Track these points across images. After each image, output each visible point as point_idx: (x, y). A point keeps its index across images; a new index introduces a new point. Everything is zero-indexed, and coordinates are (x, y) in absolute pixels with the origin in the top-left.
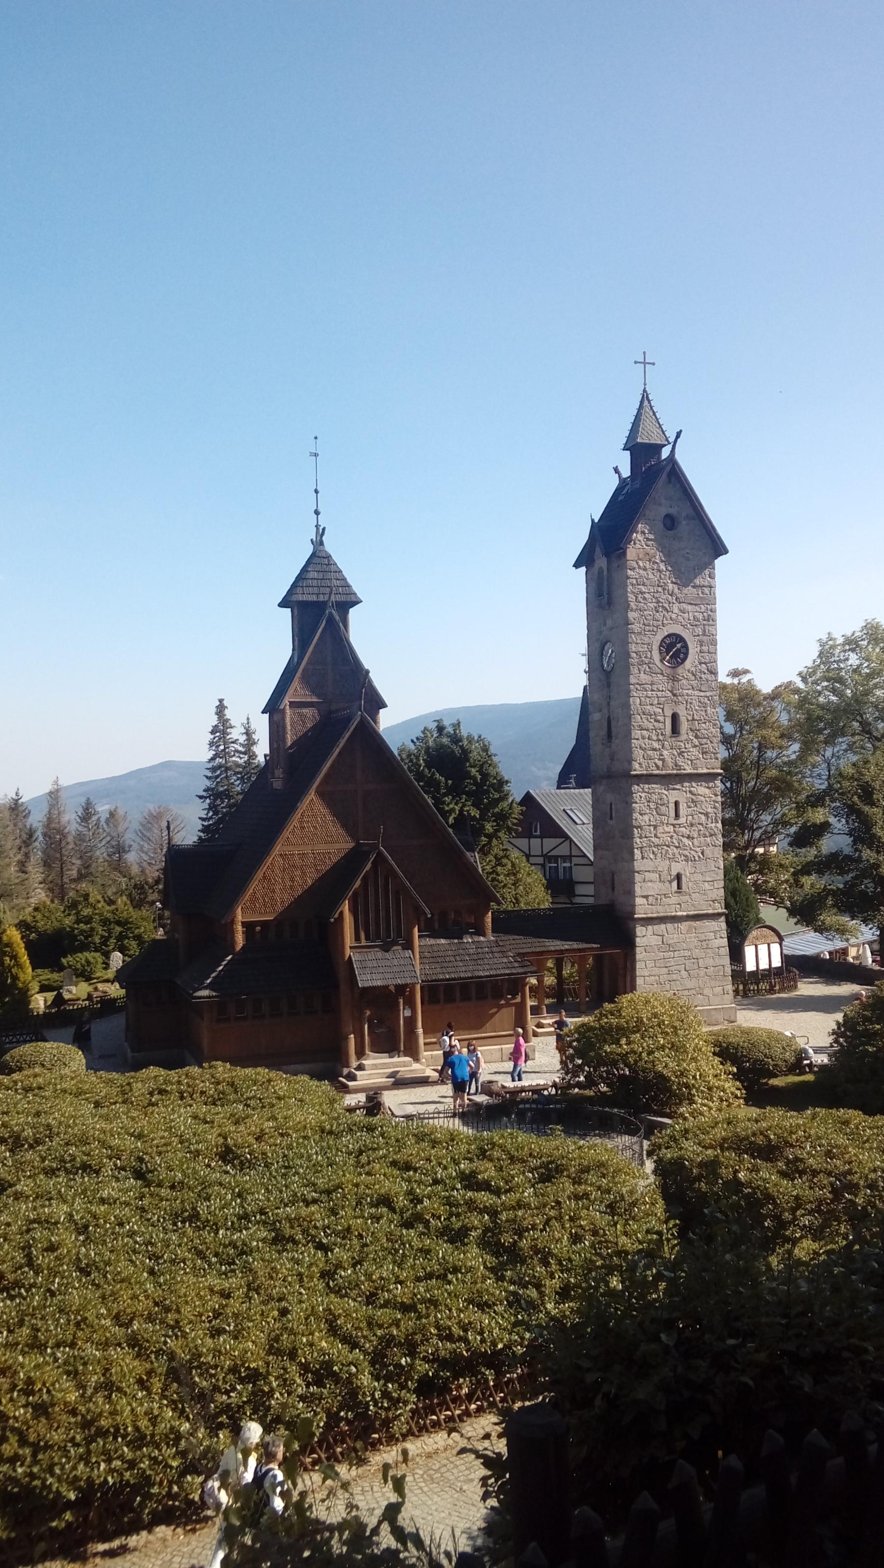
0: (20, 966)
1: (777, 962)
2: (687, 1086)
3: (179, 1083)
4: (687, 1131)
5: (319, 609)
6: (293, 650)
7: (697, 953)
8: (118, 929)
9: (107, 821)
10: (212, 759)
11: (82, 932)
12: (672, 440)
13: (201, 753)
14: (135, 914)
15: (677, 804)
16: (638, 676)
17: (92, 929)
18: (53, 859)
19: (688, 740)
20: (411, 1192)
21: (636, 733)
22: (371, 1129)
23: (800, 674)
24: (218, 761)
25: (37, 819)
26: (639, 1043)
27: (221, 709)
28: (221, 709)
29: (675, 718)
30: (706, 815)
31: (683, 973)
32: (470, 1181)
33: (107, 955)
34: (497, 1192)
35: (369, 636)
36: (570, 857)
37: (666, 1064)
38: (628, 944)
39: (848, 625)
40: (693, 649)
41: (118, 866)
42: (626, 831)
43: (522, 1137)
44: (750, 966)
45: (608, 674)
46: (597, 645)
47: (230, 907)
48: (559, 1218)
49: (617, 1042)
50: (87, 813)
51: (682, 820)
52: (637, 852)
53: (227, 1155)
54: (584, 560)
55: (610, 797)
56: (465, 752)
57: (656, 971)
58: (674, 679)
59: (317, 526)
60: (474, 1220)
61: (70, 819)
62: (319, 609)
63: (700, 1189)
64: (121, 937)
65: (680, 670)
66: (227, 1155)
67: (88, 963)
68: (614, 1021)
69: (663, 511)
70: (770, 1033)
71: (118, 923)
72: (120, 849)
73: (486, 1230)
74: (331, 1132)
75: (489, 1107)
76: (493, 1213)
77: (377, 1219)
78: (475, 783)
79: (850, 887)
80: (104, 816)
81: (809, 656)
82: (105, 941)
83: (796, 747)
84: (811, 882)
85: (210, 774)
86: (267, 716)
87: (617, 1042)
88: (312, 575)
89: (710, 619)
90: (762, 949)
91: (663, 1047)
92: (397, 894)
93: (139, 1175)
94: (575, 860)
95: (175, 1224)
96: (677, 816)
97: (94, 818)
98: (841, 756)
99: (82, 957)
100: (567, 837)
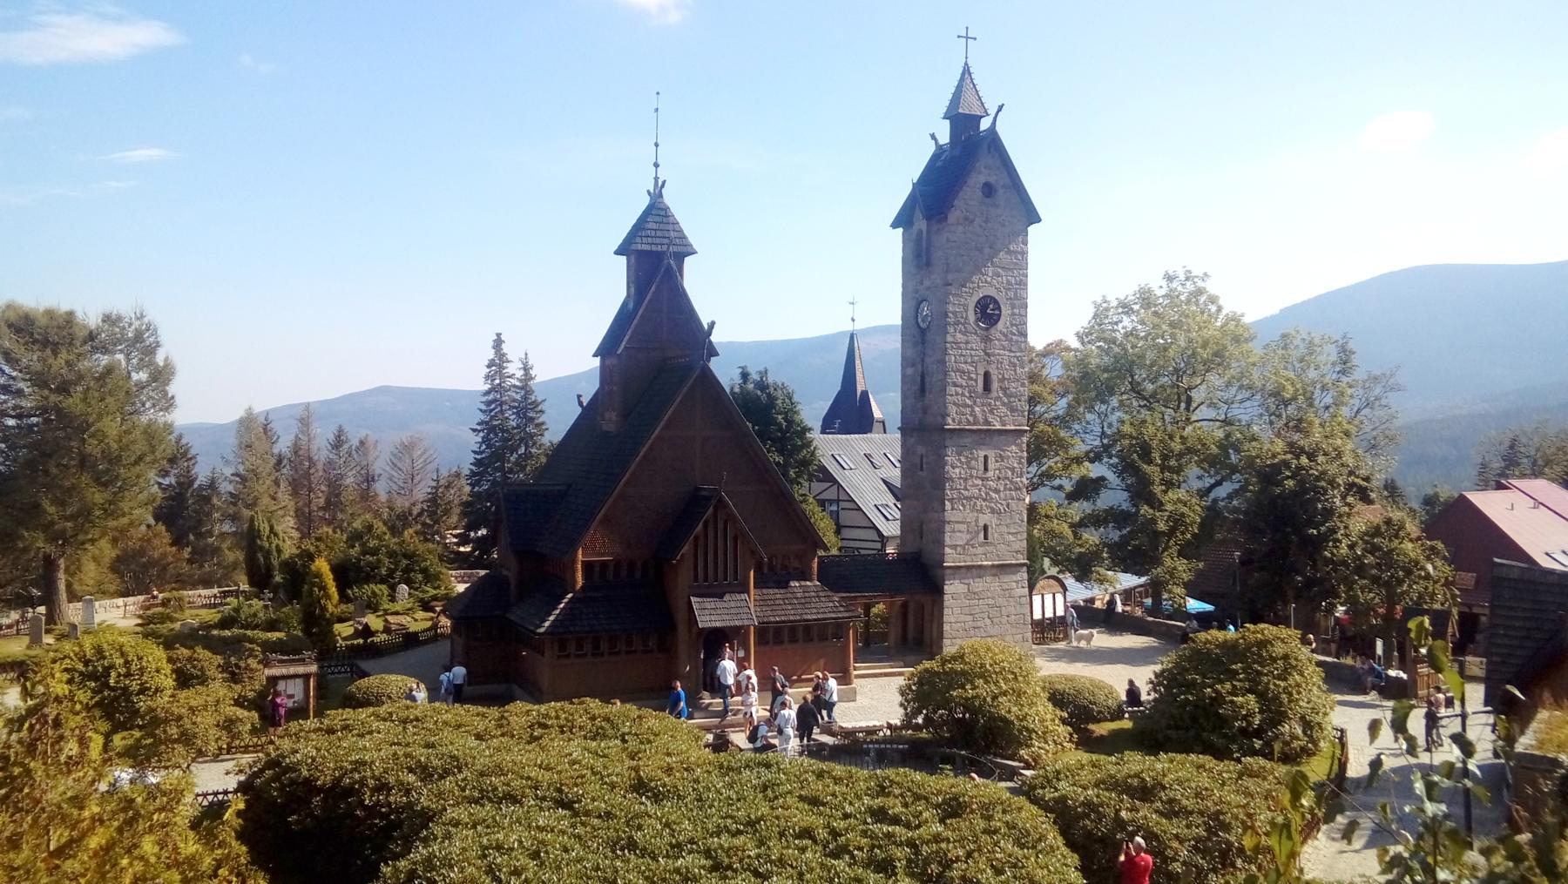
0: (328, 597)
1: (1060, 612)
2: (1027, 729)
3: (557, 717)
4: (1058, 772)
5: (655, 255)
6: (628, 295)
7: (1001, 601)
8: (405, 562)
9: (357, 450)
10: (488, 393)
11: (369, 564)
12: (992, 112)
13: (477, 383)
14: (421, 548)
15: (986, 457)
16: (955, 335)
17: (379, 561)
18: (300, 484)
19: (998, 398)
20: (828, 826)
21: (951, 390)
22: (768, 766)
23: (1077, 334)
24: (491, 397)
25: (283, 446)
26: (983, 689)
27: (498, 343)
28: (498, 343)
29: (987, 375)
30: (1013, 469)
31: (988, 621)
32: (880, 815)
33: (393, 588)
34: (908, 826)
35: (707, 288)
36: (838, 501)
37: (1007, 708)
38: (937, 591)
39: (1124, 289)
40: (1006, 311)
41: (366, 496)
42: (938, 482)
43: (918, 776)
44: (1037, 615)
45: (923, 332)
46: (914, 303)
47: (572, 545)
48: (979, 850)
49: (963, 687)
50: (338, 442)
51: (990, 474)
52: (948, 505)
53: (639, 786)
54: (903, 220)
55: (921, 450)
56: (772, 399)
57: (963, 618)
58: (986, 339)
59: (656, 179)
60: (898, 853)
61: (320, 447)
62: (655, 255)
63: (1085, 826)
64: (407, 570)
65: (993, 331)
66: (639, 786)
67: (374, 592)
68: (959, 667)
69: (982, 179)
70: (1091, 680)
71: (405, 556)
72: (370, 479)
73: (909, 861)
74: (732, 769)
75: (834, 748)
76: (911, 843)
77: (803, 850)
78: (780, 429)
79: (1124, 541)
80: (355, 443)
81: (1084, 319)
82: (391, 573)
83: (1063, 403)
84: (1091, 537)
85: (484, 407)
86: (598, 359)
87: (963, 687)
88: (651, 225)
89: (1023, 284)
90: (1048, 598)
91: (1005, 694)
92: (735, 539)
93: (562, 804)
94: (842, 505)
95: (613, 852)
96: (986, 469)
97: (346, 446)
98: (1116, 415)
99: (369, 589)
100: (835, 481)
